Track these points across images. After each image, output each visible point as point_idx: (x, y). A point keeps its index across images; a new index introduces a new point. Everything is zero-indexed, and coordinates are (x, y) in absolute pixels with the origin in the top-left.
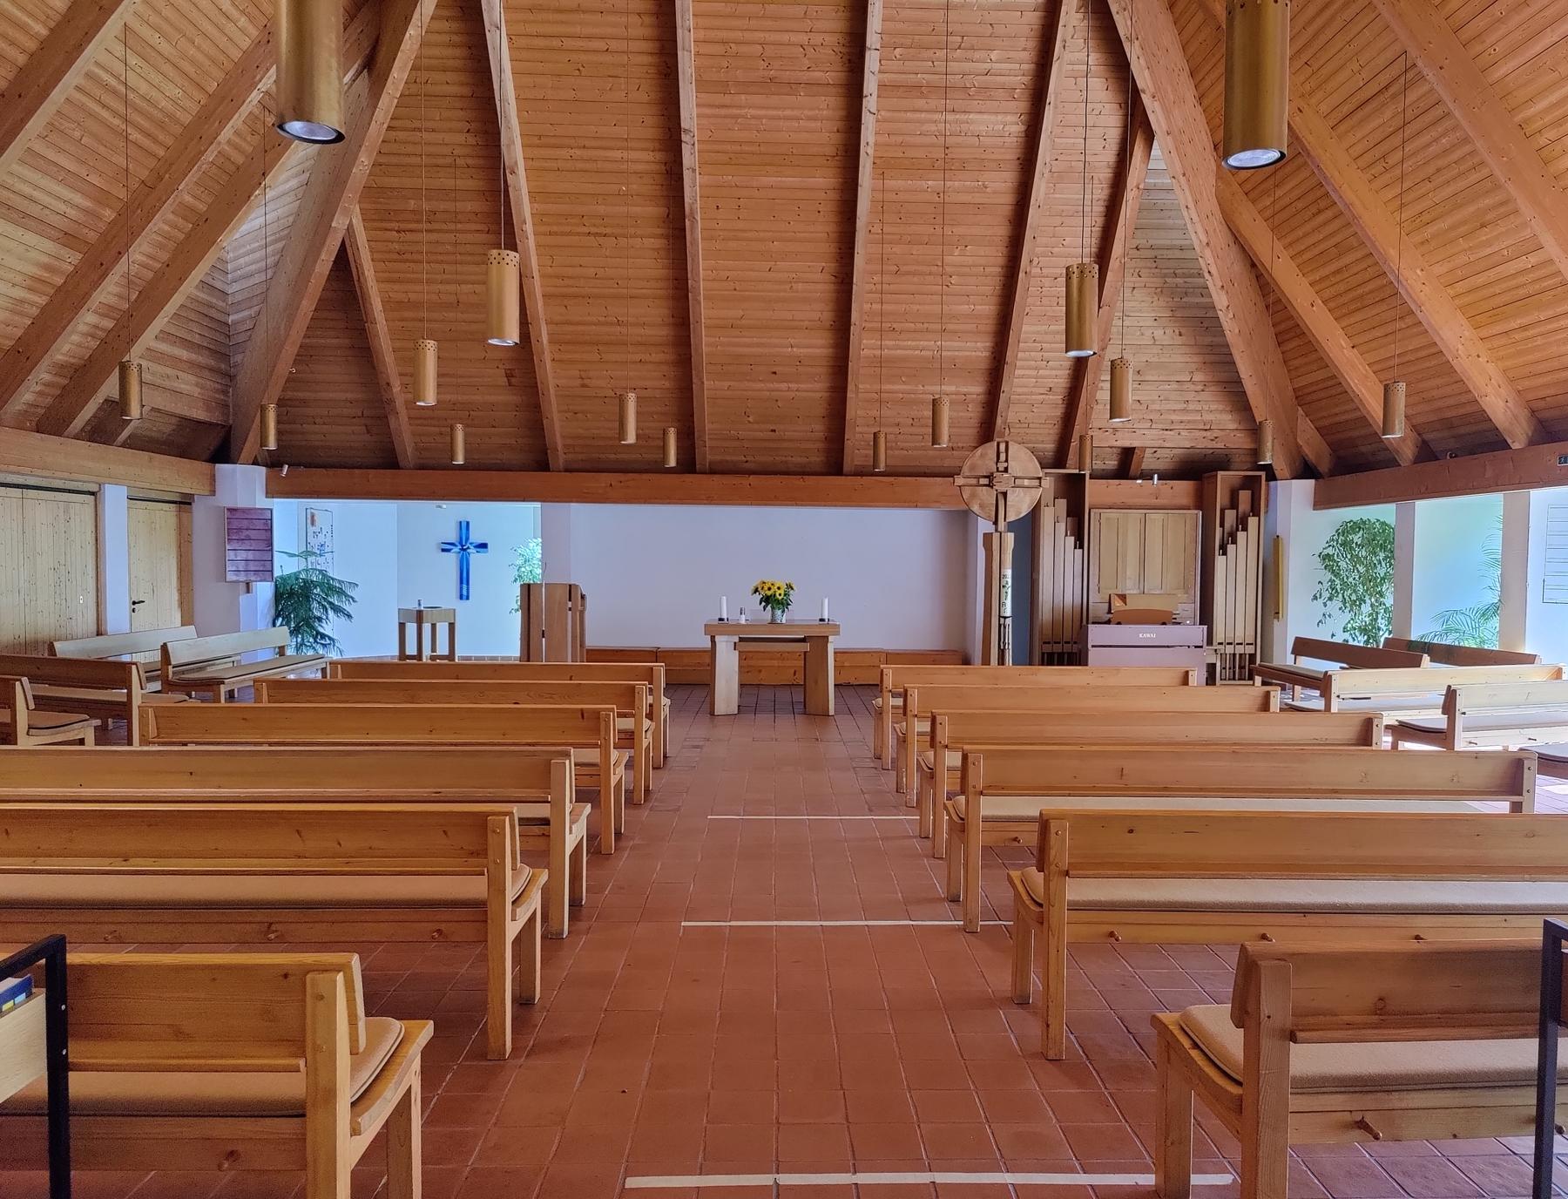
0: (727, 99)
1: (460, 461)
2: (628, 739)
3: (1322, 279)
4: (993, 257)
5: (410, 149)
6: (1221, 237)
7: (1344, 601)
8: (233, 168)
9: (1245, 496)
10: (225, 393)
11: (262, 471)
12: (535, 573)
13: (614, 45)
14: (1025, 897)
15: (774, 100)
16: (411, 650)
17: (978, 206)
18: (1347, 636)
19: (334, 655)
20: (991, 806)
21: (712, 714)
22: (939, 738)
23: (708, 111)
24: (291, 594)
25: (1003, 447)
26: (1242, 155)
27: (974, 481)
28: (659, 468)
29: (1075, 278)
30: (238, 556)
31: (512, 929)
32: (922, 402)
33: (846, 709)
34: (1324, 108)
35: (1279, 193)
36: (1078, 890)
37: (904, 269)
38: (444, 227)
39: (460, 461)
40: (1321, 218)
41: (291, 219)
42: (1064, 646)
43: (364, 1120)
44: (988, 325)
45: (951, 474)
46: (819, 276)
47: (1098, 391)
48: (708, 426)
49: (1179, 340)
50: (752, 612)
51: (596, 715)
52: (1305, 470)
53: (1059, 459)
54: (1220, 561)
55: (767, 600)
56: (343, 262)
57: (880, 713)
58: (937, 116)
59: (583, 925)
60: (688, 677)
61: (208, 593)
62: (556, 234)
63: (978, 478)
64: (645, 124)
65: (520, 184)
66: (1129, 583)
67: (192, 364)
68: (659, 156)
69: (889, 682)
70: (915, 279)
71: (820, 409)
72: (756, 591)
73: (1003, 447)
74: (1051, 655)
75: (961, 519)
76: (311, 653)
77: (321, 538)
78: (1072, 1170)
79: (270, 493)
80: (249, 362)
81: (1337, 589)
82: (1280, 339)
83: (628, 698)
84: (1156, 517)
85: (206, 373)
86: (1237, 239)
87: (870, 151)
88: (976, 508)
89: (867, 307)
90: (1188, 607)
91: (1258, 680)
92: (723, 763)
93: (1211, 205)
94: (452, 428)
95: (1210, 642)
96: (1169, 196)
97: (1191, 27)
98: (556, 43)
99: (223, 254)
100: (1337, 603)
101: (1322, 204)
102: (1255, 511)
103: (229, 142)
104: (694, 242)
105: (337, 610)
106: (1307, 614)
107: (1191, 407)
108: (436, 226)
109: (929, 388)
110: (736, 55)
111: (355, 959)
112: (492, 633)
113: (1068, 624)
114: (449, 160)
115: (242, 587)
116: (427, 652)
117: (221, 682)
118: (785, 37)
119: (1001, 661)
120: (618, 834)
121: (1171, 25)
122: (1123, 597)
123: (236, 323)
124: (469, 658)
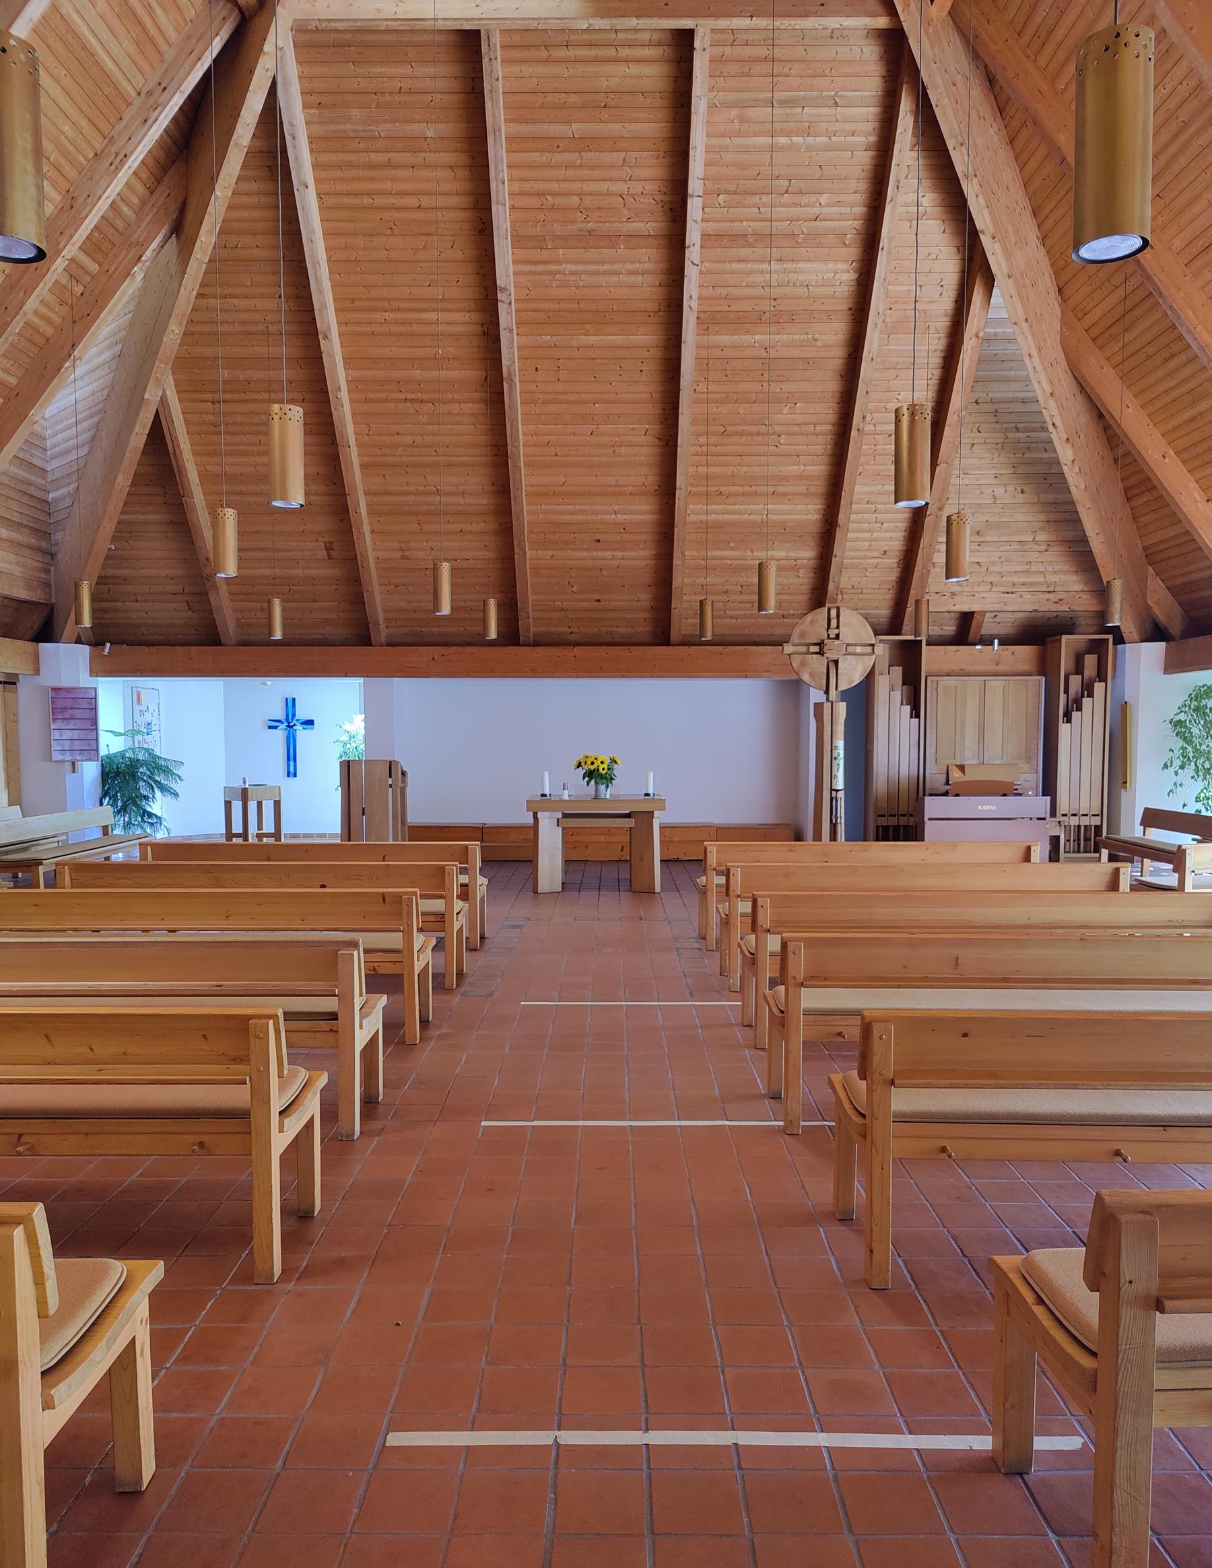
0: (544, 255)
1: (278, 635)
2: (438, 921)
3: (1175, 428)
4: (825, 413)
6: (1067, 386)
7: (1197, 770)
8: (43, 341)
9: (1090, 661)
10: (47, 571)
11: (85, 649)
12: (358, 749)
13: (425, 201)
14: (847, 1106)
15: (593, 254)
16: (237, 828)
17: (807, 360)
18: (1199, 806)
19: (160, 835)
20: (812, 999)
21: (536, 892)
22: (760, 921)
24: (118, 773)
25: (833, 613)
26: (1095, 244)
27: (804, 649)
28: (481, 641)
29: (905, 421)
30: (63, 735)
31: (280, 1142)
32: (750, 568)
33: (672, 885)
34: (1177, 243)
35: (1129, 337)
36: (904, 1100)
37: (731, 429)
38: (259, 396)
39: (278, 635)
40: (1173, 364)
41: (105, 392)
42: (896, 819)
43: (58, 1392)
44: (819, 486)
45: (779, 643)
47: (934, 551)
48: (531, 597)
49: (1020, 498)
50: (575, 788)
51: (398, 898)
52: (1155, 633)
53: (894, 625)
54: (1064, 729)
55: (590, 775)
56: (158, 434)
57: (703, 892)
58: (764, 266)
59: (375, 1125)
60: (508, 854)
61: (35, 772)
62: (372, 401)
63: (808, 645)
64: (459, 286)
65: (334, 348)
66: (968, 754)
67: (11, 541)
68: (475, 317)
69: (712, 860)
70: (743, 440)
71: (646, 578)
72: (579, 765)
73: (833, 613)
74: (886, 828)
75: (794, 688)
76: (139, 831)
78: (898, 1431)
79: (94, 672)
80: (67, 539)
81: (1191, 757)
82: (1129, 494)
83: (437, 881)
84: (996, 683)
85: (27, 552)
86: (1084, 389)
87: (694, 304)
88: (806, 677)
89: (692, 470)
90: (1031, 778)
91: (1105, 853)
92: (545, 939)
93: (1056, 353)
94: (270, 602)
95: (1053, 813)
96: (1011, 346)
97: (1033, 164)
98: (366, 201)
99: (37, 428)
100: (1190, 771)
101: (1175, 348)
102: (1101, 676)
103: (36, 312)
104: (513, 406)
105: (164, 789)
106: (1157, 783)
107: (1034, 568)
109: (757, 554)
110: (553, 208)
111: (39, 1213)
112: (314, 809)
113: (904, 798)
114: (261, 328)
115: (68, 766)
116: (253, 830)
117: (39, 862)
118: (604, 187)
119: (833, 837)
120: (424, 1023)
121: (1013, 162)
122: (962, 768)
123: (54, 500)
124: (297, 836)
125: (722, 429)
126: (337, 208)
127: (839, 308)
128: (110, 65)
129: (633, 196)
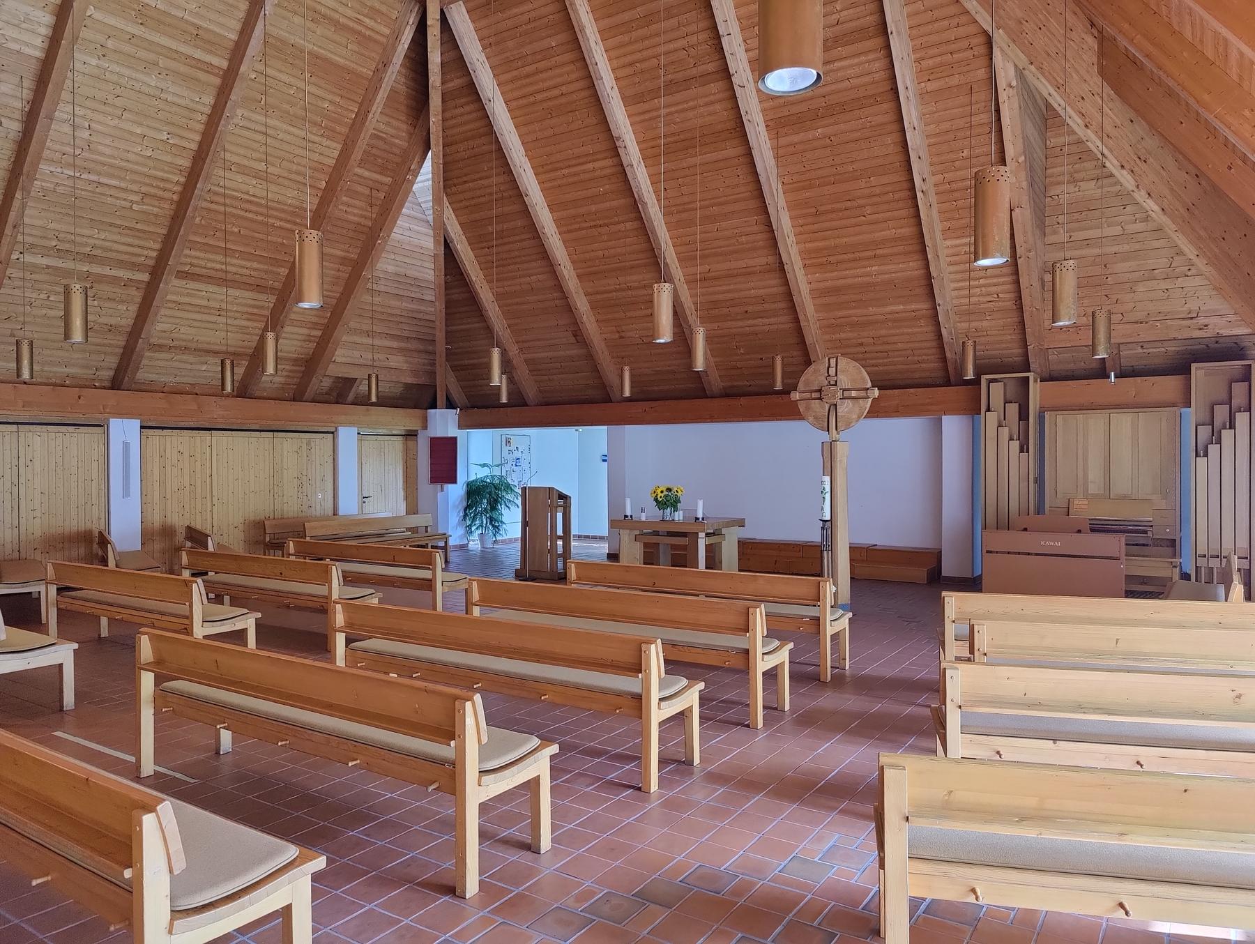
5: (478, 193)
13: (564, 89)
23: (638, 119)
37: (823, 208)
39: (627, 393)
46: (755, 229)
50: (650, 513)
67: (401, 350)
73: (833, 362)
77: (517, 454)
98: (532, 99)
108: (506, 240)
125: (814, 210)
126: (520, 107)
127: (881, 90)
128: (342, 61)
129: (692, 46)
